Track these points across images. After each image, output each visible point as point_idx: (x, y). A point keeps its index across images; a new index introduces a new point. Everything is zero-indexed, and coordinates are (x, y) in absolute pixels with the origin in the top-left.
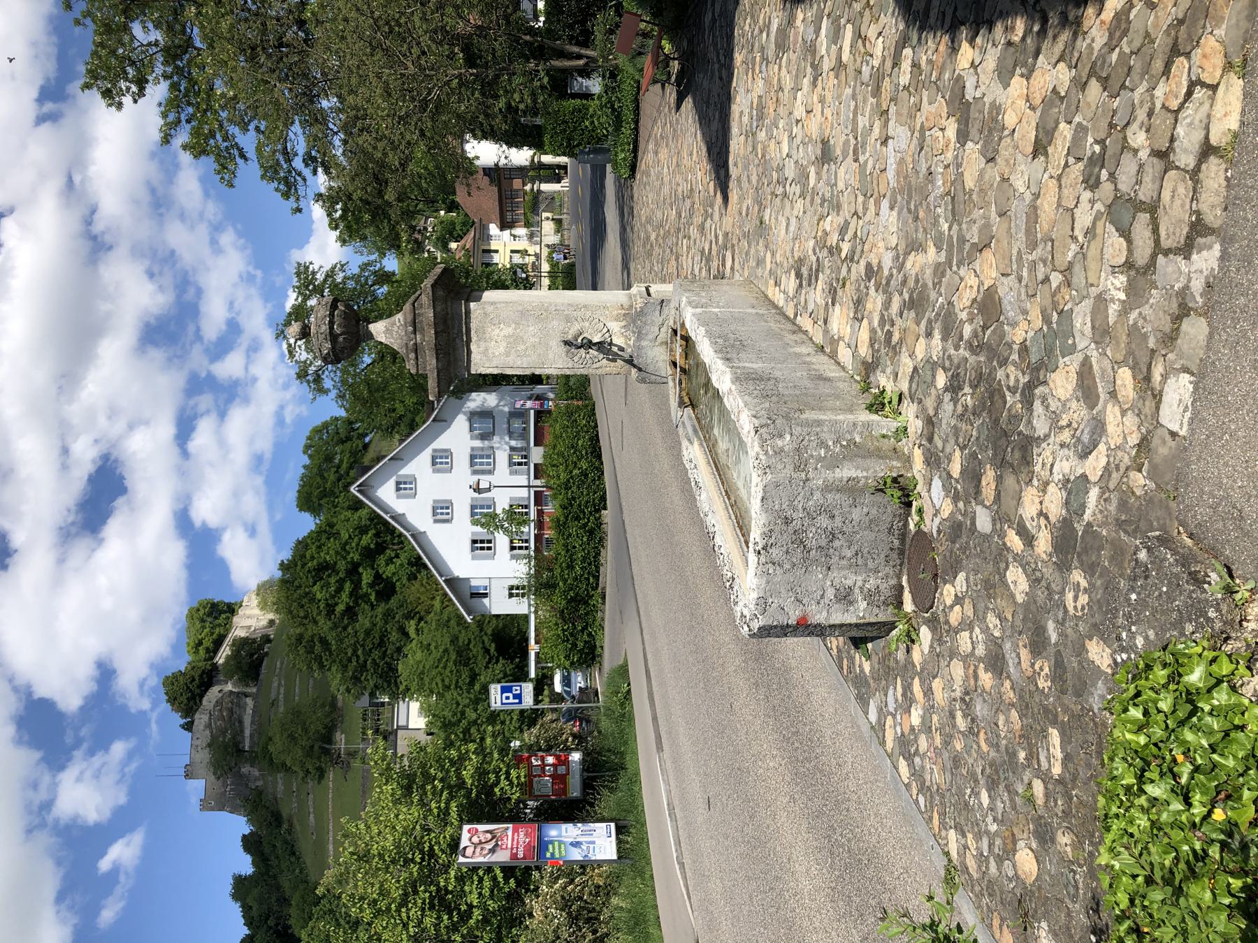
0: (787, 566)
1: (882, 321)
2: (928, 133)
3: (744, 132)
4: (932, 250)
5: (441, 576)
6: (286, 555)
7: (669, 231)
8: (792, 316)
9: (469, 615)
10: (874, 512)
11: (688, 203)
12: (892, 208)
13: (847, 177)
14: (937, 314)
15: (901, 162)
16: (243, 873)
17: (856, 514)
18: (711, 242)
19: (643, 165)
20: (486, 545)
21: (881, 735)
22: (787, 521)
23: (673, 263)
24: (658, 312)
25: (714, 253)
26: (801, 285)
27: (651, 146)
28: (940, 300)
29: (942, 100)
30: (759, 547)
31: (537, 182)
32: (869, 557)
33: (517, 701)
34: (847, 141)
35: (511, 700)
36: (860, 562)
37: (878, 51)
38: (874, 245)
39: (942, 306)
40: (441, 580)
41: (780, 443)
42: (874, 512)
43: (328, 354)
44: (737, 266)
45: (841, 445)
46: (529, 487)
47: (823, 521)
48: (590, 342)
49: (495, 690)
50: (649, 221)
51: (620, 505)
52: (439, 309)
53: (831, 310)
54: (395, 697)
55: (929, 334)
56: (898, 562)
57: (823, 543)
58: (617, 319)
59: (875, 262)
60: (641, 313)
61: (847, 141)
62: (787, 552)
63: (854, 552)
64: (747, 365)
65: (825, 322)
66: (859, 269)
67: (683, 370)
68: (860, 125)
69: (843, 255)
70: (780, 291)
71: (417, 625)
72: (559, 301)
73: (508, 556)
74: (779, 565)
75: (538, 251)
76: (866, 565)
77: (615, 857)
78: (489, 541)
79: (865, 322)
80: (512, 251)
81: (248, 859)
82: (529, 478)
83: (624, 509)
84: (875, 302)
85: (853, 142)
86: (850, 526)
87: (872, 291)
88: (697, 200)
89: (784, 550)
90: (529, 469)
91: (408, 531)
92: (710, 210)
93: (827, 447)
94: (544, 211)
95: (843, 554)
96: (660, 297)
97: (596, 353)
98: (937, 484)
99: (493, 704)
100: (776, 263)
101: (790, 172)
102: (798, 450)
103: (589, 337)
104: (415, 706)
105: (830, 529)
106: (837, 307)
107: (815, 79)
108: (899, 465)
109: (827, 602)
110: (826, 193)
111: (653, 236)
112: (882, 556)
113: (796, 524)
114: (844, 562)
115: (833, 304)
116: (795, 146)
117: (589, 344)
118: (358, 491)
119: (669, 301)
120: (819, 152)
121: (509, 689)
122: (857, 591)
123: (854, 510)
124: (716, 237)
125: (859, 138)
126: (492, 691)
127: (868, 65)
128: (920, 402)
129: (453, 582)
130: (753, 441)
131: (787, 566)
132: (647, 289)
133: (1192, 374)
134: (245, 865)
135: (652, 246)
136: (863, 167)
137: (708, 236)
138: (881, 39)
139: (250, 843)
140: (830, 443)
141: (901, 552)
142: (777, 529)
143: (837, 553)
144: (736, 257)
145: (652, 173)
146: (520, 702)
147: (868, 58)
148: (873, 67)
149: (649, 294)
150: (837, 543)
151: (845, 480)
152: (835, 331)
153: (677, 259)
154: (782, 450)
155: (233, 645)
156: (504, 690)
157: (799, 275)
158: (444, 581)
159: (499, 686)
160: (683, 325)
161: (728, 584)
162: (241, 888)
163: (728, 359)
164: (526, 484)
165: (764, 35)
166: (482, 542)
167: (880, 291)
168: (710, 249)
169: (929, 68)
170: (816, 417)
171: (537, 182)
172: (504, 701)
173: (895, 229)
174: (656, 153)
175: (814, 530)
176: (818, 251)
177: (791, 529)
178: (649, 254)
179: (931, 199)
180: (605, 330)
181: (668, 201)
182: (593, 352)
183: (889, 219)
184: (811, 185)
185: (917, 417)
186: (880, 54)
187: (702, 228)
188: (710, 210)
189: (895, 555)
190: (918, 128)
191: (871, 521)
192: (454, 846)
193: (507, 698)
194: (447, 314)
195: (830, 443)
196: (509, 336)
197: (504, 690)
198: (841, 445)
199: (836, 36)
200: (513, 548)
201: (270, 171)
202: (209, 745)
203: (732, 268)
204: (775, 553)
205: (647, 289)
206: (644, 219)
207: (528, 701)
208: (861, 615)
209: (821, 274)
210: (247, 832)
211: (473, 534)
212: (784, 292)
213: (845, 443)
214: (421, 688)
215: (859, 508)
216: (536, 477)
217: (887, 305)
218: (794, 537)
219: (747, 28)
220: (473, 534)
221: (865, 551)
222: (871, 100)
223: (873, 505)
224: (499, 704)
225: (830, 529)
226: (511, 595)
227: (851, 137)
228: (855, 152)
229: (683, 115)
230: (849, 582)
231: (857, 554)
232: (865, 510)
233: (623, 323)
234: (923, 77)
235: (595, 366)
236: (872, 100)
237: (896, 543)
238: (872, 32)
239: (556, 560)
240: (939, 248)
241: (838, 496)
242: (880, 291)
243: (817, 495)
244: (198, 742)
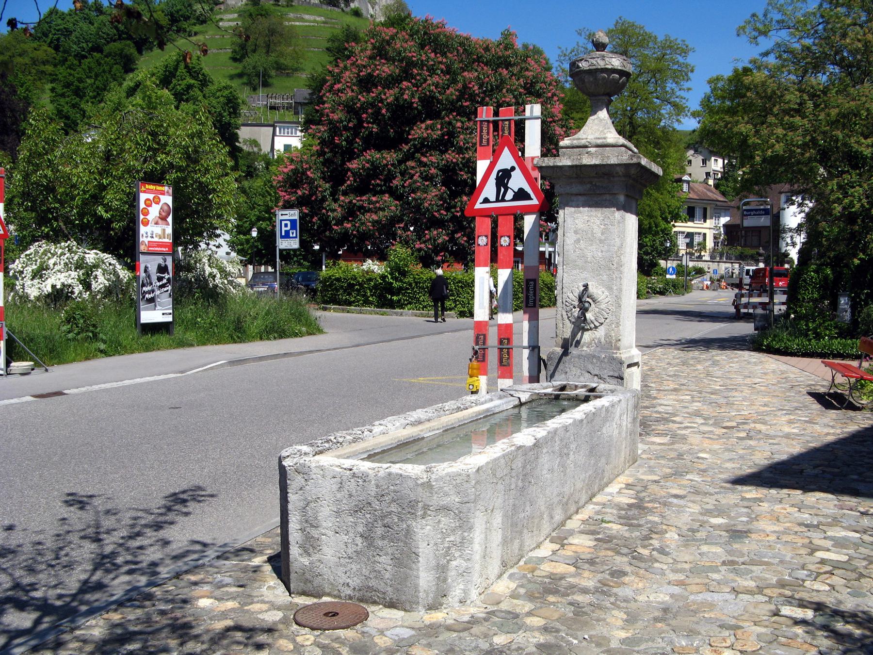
0: (339, 495)
2: (732, 632)
4: (623, 634)
8: (594, 500)
11: (722, 401)
12: (672, 596)
13: (711, 554)
14: (563, 638)
15: (712, 606)
23: (672, 386)
24: (611, 373)
25: (671, 425)
26: (622, 509)
28: (575, 642)
29: (759, 647)
30: (355, 470)
33: (283, 234)
34: (743, 555)
35: (284, 229)
37: (817, 586)
38: (642, 578)
39: (570, 644)
43: (578, 67)
44: (653, 447)
48: (587, 310)
49: (294, 214)
50: (715, 363)
51: (460, 330)
52: (618, 169)
55: (545, 629)
58: (607, 336)
59: (626, 579)
61: (743, 555)
63: (351, 555)
66: (621, 562)
67: (557, 397)
68: (754, 568)
72: (625, 282)
75: (704, 258)
77: (142, 321)
79: (572, 569)
80: (705, 235)
83: (456, 333)
84: (588, 580)
85: (741, 560)
87: (600, 576)
88: (723, 410)
92: (711, 422)
96: (626, 376)
97: (576, 314)
98: (406, 633)
99: (281, 213)
103: (590, 309)
106: (592, 543)
107: (807, 526)
109: (308, 529)
110: (700, 534)
111: (699, 367)
112: (348, 580)
115: (596, 540)
116: (751, 504)
117: (584, 310)
119: (622, 385)
120: (739, 528)
121: (293, 227)
124: (687, 427)
125: (743, 566)
126: (292, 212)
127: (807, 576)
128: (486, 619)
131: (339, 495)
132: (636, 364)
136: (715, 570)
137: (688, 420)
138: (827, 588)
146: (282, 237)
147: (813, 577)
148: (804, 581)
149: (629, 366)
151: (416, 552)
153: (675, 390)
156: (293, 222)
159: (296, 217)
160: (596, 397)
161: (332, 438)
165: (855, 477)
167: (599, 585)
168: (674, 422)
169: (790, 635)
172: (283, 223)
173: (651, 598)
178: (684, 363)
179: (674, 636)
180: (597, 324)
181: (729, 382)
182: (576, 312)
183: (662, 596)
185: (472, 617)
186: (815, 587)
187: (697, 414)
188: (711, 422)
190: (741, 624)
193: (286, 225)
194: (613, 177)
196: (593, 233)
197: (293, 222)
199: (840, 544)
203: (653, 443)
205: (636, 364)
206: (718, 358)
207: (283, 244)
209: (627, 528)
215: (390, 562)
217: (585, 591)
219: (866, 460)
222: (775, 579)
227: (746, 558)
228: (732, 563)
229: (801, 399)
231: (350, 558)
233: (603, 340)
234: (784, 629)
235: (564, 313)
236: (774, 580)
238: (836, 580)
239: (254, 303)
240: (623, 641)
242: (599, 585)
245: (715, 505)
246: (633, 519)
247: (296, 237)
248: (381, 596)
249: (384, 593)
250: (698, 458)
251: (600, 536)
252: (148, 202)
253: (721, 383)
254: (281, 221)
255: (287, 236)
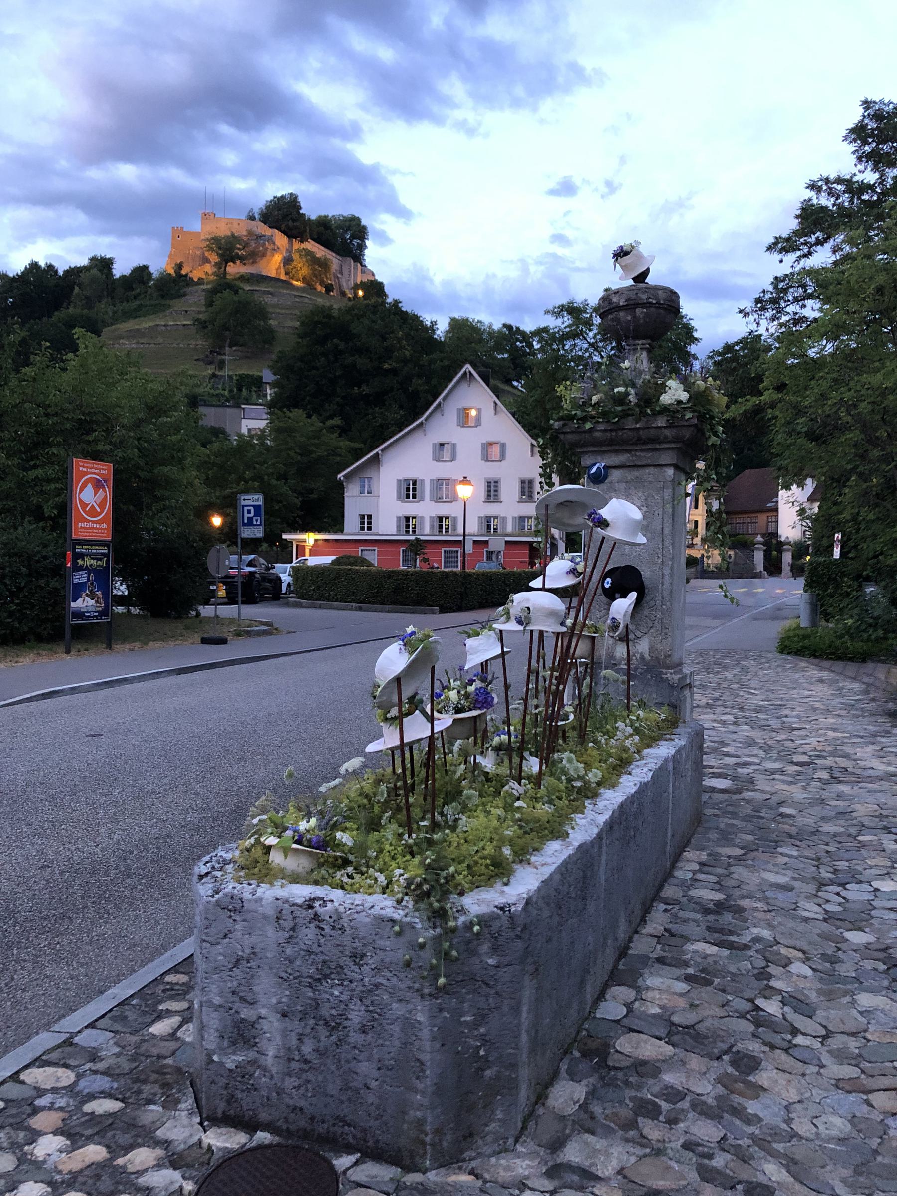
1: (674, 1095)
3: (885, 813)
5: (383, 450)
6: (405, 307)
7: (737, 695)
9: (344, 476)
10: (371, 1098)
16: (114, 266)
17: (366, 1068)
18: (738, 757)
19: (803, 664)
20: (411, 493)
21: (54, 1056)
22: (357, 957)
23: (704, 701)
26: (706, 912)
27: (825, 674)
31: (765, 548)
32: (301, 1081)
33: (246, 521)
35: (246, 515)
36: (294, 1065)
40: (378, 450)
41: (485, 948)
42: (371, 1098)
45: (478, 1048)
46: (464, 535)
47: (356, 1015)
49: (257, 499)
53: (678, 972)
54: (270, 405)
56: (293, 1127)
57: (325, 1011)
60: (660, 680)
62: (310, 952)
63: (308, 1057)
64: (604, 858)
65: (661, 961)
69: (760, 1002)
70: (694, 872)
71: (338, 426)
73: (400, 515)
74: (290, 937)
76: (289, 1075)
78: (414, 497)
81: (127, 272)
82: (474, 535)
86: (350, 1057)
89: (315, 948)
90: (484, 535)
91: (426, 420)
93: (476, 1025)
94: (736, 554)
95: (306, 1040)
99: (243, 498)
100: (729, 865)
101: (856, 893)
102: (473, 979)
104: (262, 424)
105: (346, 1023)
108: (445, 1144)
112: (303, 1103)
113: (352, 971)
114: (294, 1041)
118: (465, 373)
122: (252, 1055)
123: (375, 1065)
129: (376, 460)
130: (488, 904)
131: (288, 951)
133: (554, 1077)
134: (121, 269)
135: (718, 672)
137: (746, 751)
139: (141, 272)
140: (482, 1030)
141: (306, 1135)
142: (347, 940)
143: (308, 1030)
144: (726, 796)
145: (797, 676)
146: (244, 525)
150: (323, 1032)
152: (649, 982)
154: (473, 953)
155: (326, 259)
157: (720, 907)
158: (377, 453)
159: (260, 503)
162: (103, 264)
163: (611, 828)
164: (467, 533)
166: (408, 490)
168: (728, 755)
170: (525, 1000)
171: (765, 548)
172: (246, 509)
174: (821, 681)
175: (345, 997)
176: (759, 946)
177: (347, 961)
184: (848, 935)
189: (303, 1123)
191: (357, 1091)
192: (96, 456)
193: (249, 512)
195: (482, 1030)
198: (478, 1048)
200: (407, 519)
201: (781, 285)
202: (233, 235)
204: (308, 934)
207: (246, 533)
208: (215, 1058)
210: (152, 269)
211: (422, 481)
212: (695, 880)
213: (482, 1053)
214: (277, 430)
215: (375, 1074)
216: (475, 542)
218: (333, 965)
220: (422, 481)
221: (310, 1076)
223: (380, 1098)
224: (243, 503)
225: (346, 1023)
226: (362, 517)
230: (263, 1044)
232: (374, 1084)
233: (647, 656)
237: (321, 1129)
241: (397, 1043)
243: (398, 1009)
244: (235, 225)
245: (840, 904)
246: (731, 933)
247: (260, 525)
248: (359, 1135)
249: (364, 1130)
250: (781, 815)
251: (690, 971)
252: (495, 451)
253: (763, 697)
254: (244, 506)
255: (250, 523)
